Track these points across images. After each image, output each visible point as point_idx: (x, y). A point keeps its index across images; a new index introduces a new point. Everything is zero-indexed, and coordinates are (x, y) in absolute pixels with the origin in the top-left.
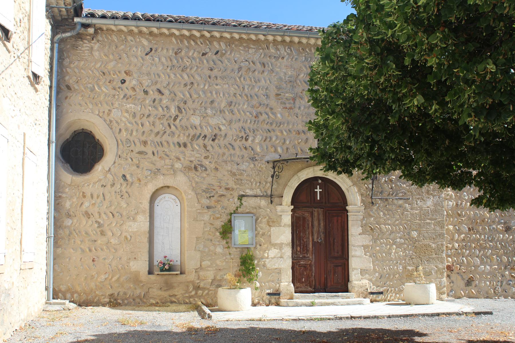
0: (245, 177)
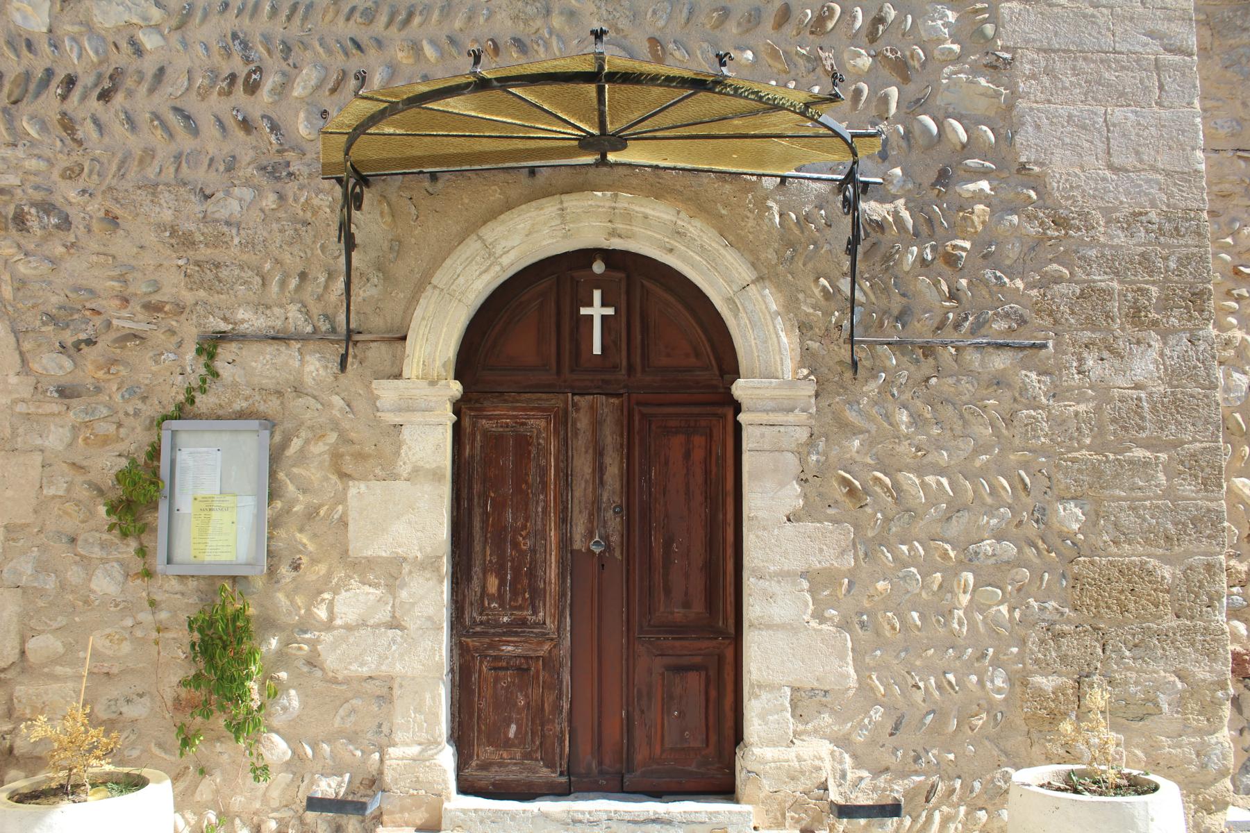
0: (234, 251)
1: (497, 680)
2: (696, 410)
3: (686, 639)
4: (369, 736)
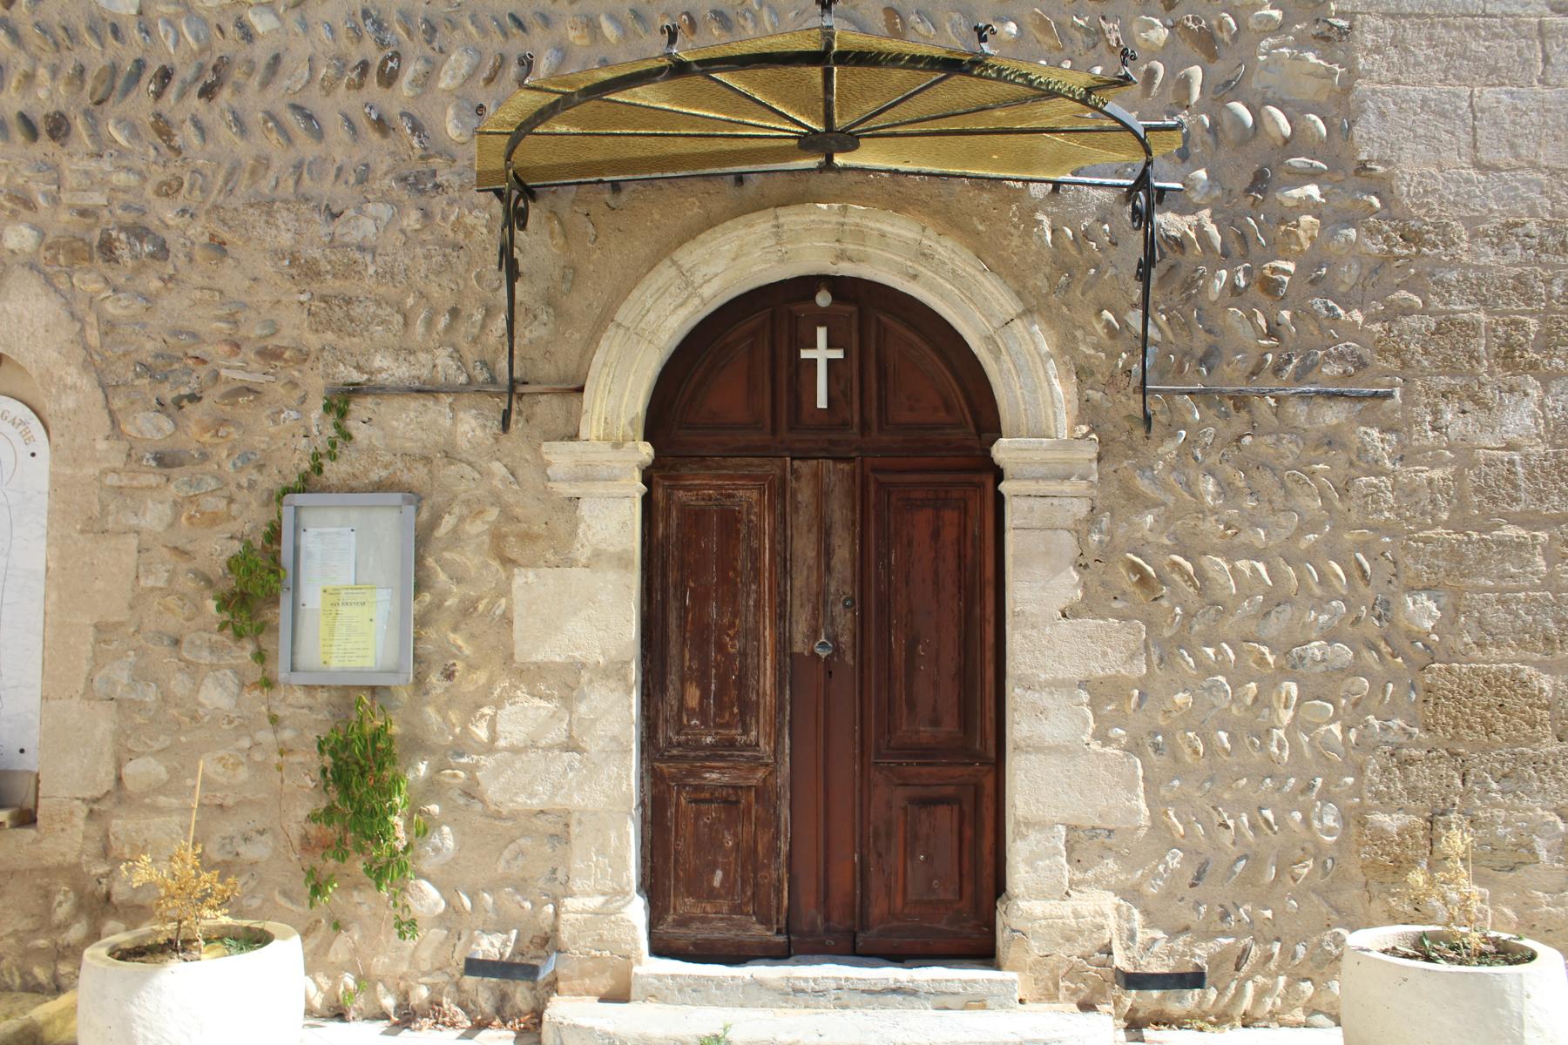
0: (369, 283)
2: (947, 478)
4: (541, 884)
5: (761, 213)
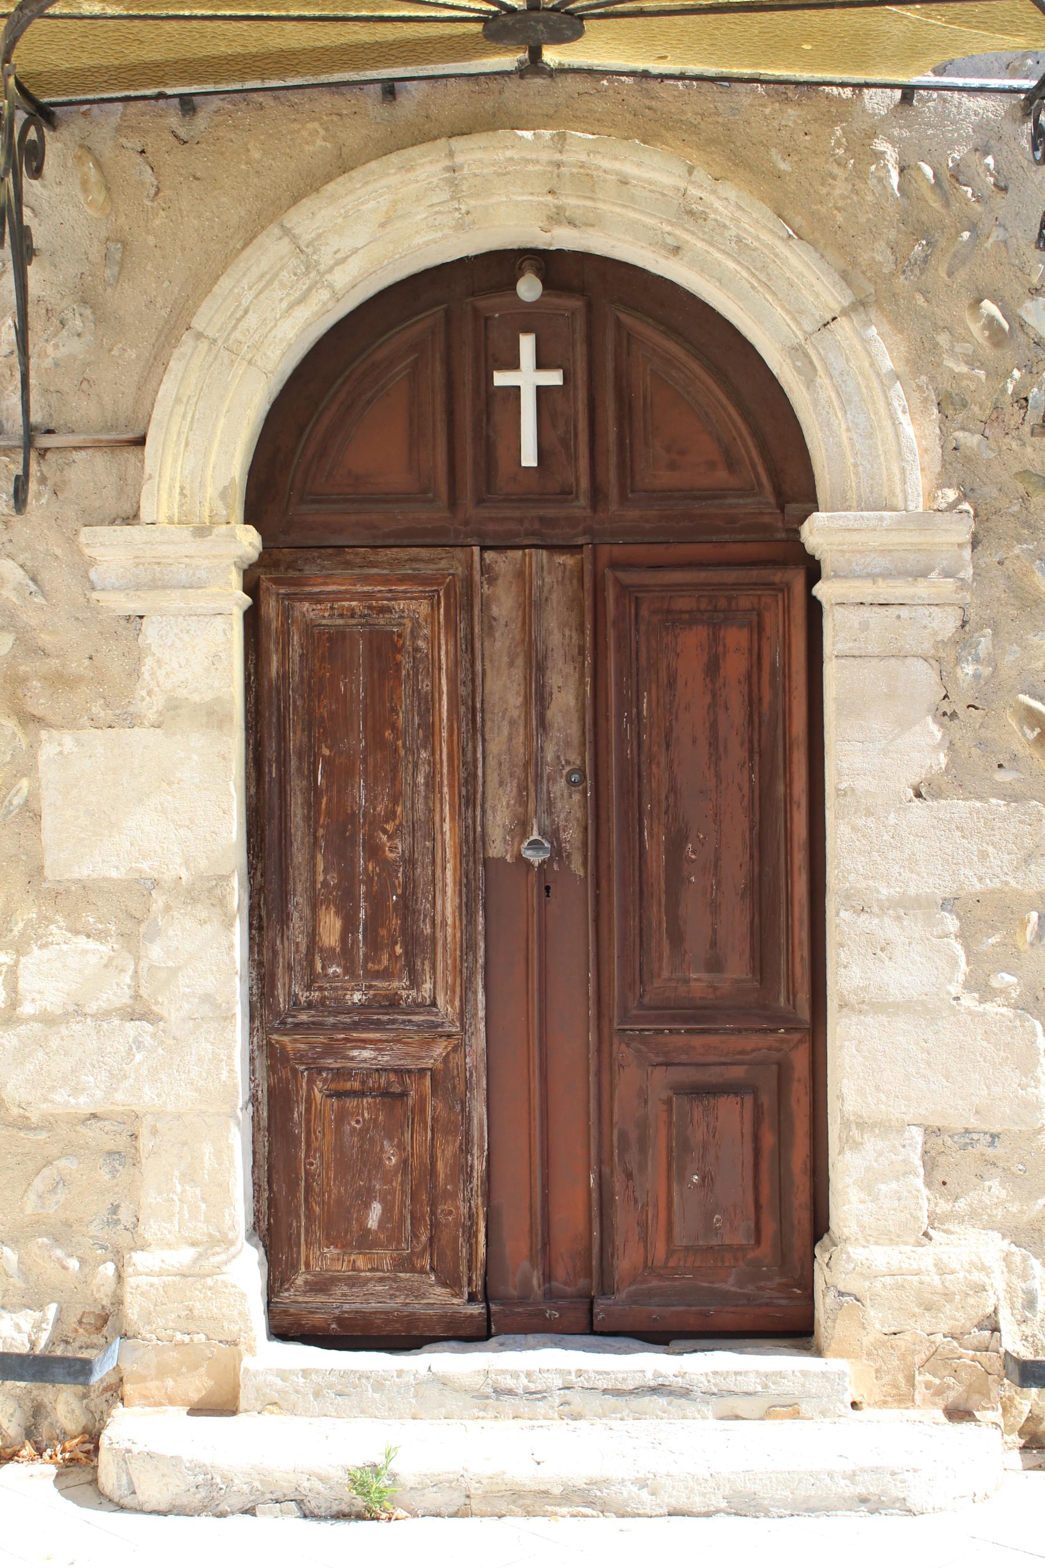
1: (342, 1117)
2: (730, 576)
3: (716, 1031)
4: (94, 1230)
5: (425, 147)
